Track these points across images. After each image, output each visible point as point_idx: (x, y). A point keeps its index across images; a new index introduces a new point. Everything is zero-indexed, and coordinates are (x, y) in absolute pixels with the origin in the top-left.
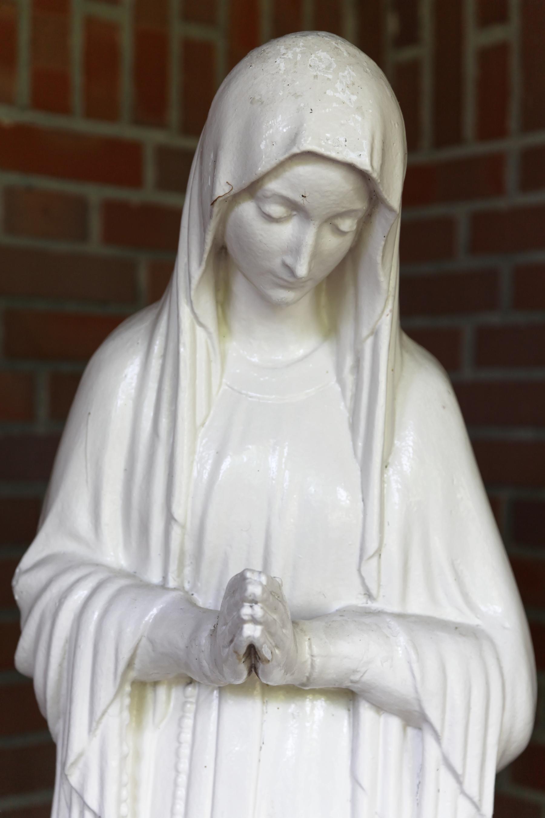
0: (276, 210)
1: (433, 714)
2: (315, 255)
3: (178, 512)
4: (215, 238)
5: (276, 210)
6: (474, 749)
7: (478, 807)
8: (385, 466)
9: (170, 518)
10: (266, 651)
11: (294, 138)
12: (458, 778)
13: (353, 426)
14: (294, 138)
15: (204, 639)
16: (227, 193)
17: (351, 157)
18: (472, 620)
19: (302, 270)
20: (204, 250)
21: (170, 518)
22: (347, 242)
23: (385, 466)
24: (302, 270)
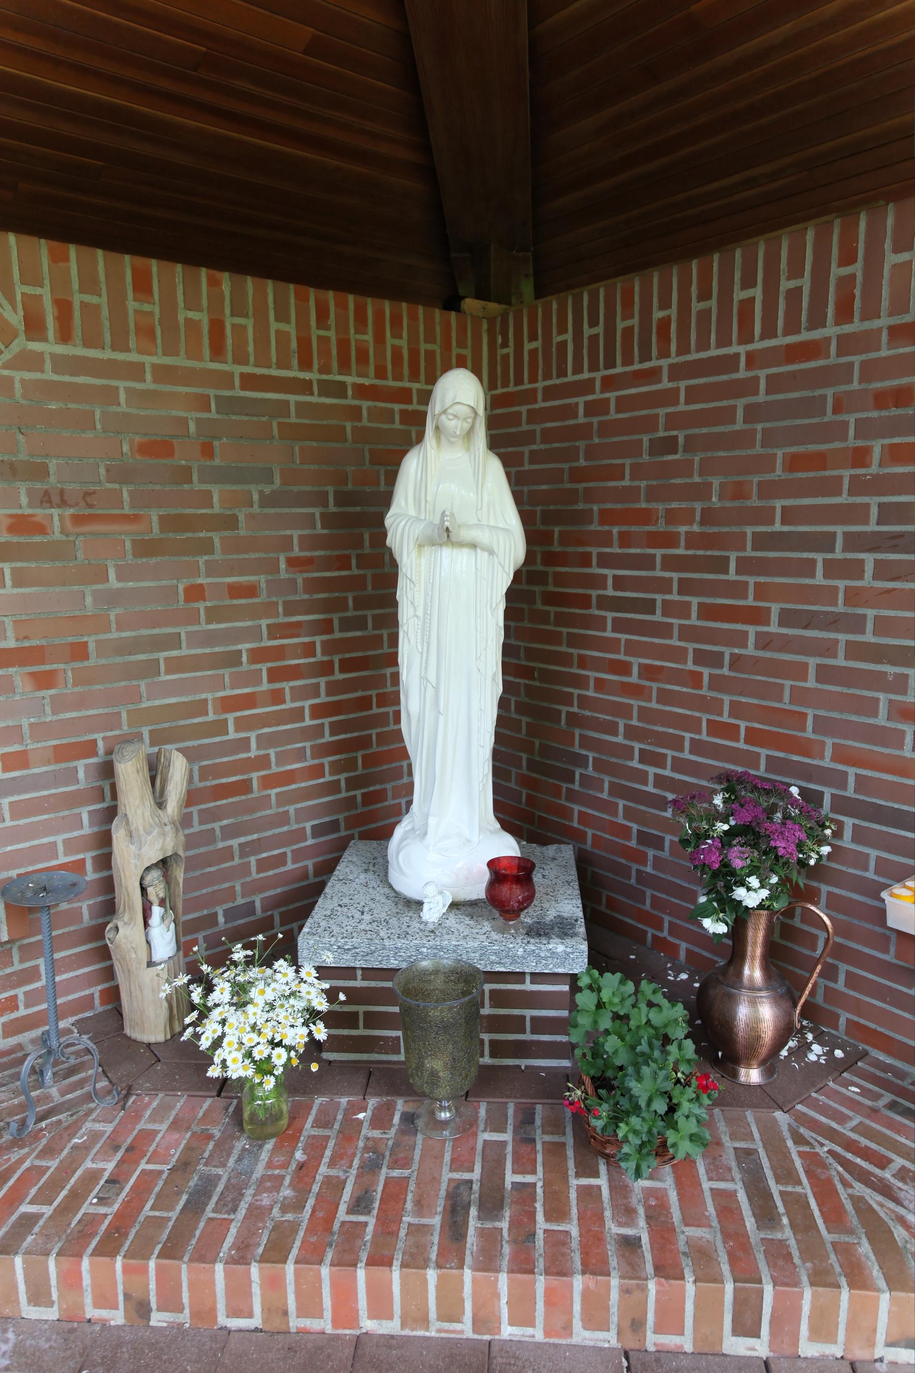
0: (451, 417)
1: (496, 551)
2: (462, 428)
3: (428, 499)
4: (197, 1213)
5: (451, 417)
6: (507, 560)
7: (508, 575)
8: (482, 486)
9: (426, 501)
10: (451, 529)
11: (454, 399)
12: (503, 567)
13: (474, 475)
14: (454, 399)
15: (436, 530)
16: (393, 889)
17: (469, 403)
18: (507, 527)
19: (458, 433)
20: (76, 1121)
21: (426, 501)
22: (470, 425)
23: (482, 486)
24: (458, 433)
